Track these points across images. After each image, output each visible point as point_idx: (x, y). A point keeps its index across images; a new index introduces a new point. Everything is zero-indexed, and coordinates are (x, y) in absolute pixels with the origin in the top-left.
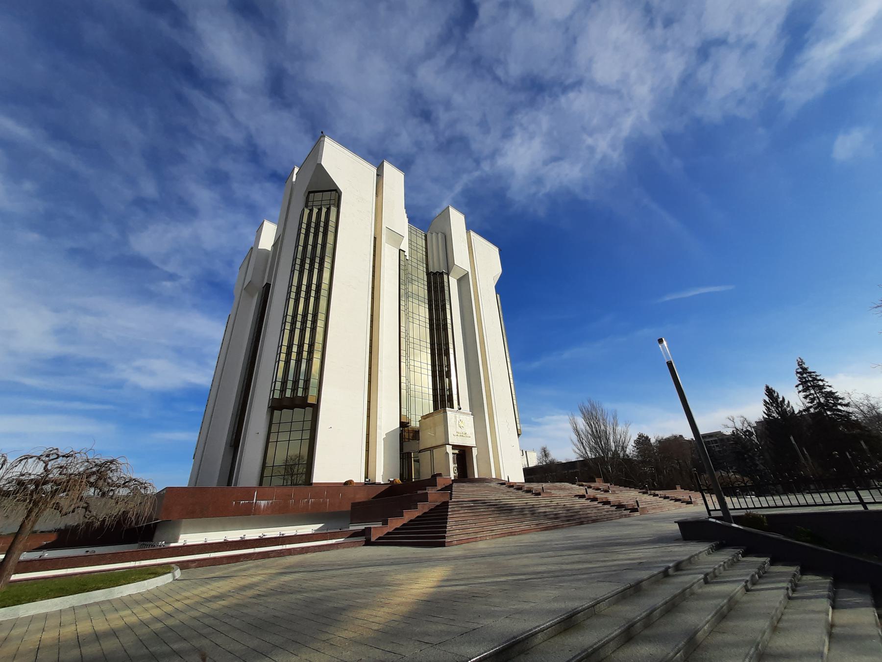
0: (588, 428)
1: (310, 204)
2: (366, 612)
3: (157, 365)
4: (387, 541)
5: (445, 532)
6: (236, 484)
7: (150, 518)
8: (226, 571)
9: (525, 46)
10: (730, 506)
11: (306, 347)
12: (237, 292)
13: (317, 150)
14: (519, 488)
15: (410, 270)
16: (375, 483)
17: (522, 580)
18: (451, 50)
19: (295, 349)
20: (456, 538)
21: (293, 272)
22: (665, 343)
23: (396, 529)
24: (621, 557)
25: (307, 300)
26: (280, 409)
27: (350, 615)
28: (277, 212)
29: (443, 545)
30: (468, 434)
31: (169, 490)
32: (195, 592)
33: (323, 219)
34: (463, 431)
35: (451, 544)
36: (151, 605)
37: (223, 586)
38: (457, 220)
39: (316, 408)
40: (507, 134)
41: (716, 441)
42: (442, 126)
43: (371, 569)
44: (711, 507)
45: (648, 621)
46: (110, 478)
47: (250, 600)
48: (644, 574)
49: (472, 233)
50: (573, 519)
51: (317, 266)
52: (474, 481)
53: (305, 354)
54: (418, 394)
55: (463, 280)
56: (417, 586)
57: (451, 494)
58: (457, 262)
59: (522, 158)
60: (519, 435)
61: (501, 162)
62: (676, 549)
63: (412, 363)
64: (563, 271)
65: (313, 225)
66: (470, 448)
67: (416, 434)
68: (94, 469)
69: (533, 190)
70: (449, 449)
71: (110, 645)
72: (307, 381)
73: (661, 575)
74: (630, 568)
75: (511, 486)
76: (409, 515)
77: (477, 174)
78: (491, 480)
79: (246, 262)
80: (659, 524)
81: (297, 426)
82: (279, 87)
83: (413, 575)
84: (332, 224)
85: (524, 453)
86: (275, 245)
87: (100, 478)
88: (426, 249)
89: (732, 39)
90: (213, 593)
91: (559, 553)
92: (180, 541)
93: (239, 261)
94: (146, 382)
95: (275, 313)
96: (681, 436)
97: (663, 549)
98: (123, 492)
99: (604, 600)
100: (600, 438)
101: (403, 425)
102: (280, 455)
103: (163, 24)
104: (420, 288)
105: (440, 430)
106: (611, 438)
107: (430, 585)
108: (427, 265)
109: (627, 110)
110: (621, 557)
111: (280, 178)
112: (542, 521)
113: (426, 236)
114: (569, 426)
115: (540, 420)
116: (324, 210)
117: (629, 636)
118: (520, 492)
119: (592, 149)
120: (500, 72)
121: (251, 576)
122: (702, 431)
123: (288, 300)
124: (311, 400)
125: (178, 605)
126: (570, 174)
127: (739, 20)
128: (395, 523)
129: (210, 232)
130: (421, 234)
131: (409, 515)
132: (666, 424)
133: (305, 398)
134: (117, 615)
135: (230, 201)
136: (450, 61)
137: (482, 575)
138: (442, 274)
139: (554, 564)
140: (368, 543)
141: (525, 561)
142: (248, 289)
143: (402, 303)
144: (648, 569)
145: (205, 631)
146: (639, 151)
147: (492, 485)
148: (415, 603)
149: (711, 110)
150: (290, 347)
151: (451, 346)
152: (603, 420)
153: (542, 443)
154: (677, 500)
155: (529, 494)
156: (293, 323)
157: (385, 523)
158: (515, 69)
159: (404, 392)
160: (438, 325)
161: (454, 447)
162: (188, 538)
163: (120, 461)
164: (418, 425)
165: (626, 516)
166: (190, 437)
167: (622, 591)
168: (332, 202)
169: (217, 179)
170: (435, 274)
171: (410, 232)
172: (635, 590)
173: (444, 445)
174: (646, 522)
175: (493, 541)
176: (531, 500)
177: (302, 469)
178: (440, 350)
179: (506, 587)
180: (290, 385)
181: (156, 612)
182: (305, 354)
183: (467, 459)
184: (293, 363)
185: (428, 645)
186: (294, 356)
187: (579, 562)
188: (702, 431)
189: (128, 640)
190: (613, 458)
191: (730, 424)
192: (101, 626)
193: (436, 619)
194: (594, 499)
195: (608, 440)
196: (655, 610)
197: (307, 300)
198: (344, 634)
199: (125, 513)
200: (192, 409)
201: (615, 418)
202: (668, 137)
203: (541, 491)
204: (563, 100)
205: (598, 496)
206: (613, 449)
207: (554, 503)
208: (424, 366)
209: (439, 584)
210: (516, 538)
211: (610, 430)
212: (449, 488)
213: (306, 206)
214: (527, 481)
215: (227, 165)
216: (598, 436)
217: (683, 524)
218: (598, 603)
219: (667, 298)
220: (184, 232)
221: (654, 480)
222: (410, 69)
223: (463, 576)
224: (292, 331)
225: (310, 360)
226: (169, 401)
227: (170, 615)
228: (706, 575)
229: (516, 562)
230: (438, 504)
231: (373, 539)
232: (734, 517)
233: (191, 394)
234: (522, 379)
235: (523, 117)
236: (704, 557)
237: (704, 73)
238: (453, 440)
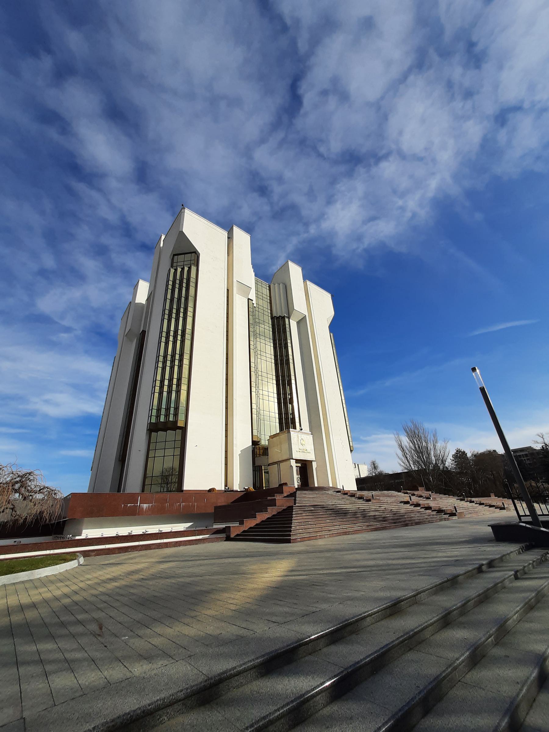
0: (411, 444)
1: (175, 264)
2: (226, 595)
3: (60, 398)
4: (243, 537)
5: (290, 531)
6: (124, 490)
7: (60, 517)
8: (117, 560)
9: (342, 126)
10: (539, 512)
11: (175, 381)
12: (120, 340)
13: (178, 219)
14: (353, 495)
15: (257, 316)
16: (233, 491)
17: (354, 572)
18: (280, 135)
19: (166, 382)
20: (299, 536)
21: (163, 320)
22: (478, 371)
23: (251, 528)
24: (440, 554)
25: (175, 343)
26: (156, 431)
27: (213, 597)
28: (148, 274)
29: (289, 541)
30: (309, 450)
31: (74, 495)
32: (95, 575)
33: (185, 276)
34: (304, 447)
35: (295, 541)
36: (62, 584)
37: (116, 571)
38: (295, 272)
39: (184, 430)
40: (330, 201)
41: (526, 455)
42: (275, 198)
43: (230, 560)
44: (522, 513)
45: (464, 609)
46: (29, 486)
47: (136, 583)
48: (460, 570)
49: (308, 283)
50: (400, 521)
51: (181, 315)
52: (314, 489)
53: (174, 387)
54: (267, 418)
55: (302, 322)
56: (267, 575)
57: (295, 500)
59: (344, 219)
60: (351, 451)
61: (325, 225)
62: (489, 549)
63: (261, 392)
64: (389, 311)
66: (311, 462)
68: (18, 479)
69: (354, 246)
70: (293, 463)
71: (31, 615)
72: (177, 409)
73: (475, 571)
74: (448, 564)
75: (345, 493)
76: (261, 517)
77: (305, 235)
78: (328, 489)
79: (127, 311)
80: (475, 527)
81: (170, 445)
82: (143, 175)
83: (263, 566)
84: (193, 280)
85: (356, 466)
86: (148, 300)
87: (22, 486)
88: (270, 297)
89: (526, 105)
90: (109, 576)
91: (386, 550)
92: (83, 535)
93: (119, 315)
94: (53, 411)
95: (150, 353)
96: (495, 451)
97: (477, 549)
98: (39, 496)
99: (424, 591)
100: (422, 453)
101: (255, 443)
103: (53, 133)
104: (267, 328)
105: (285, 446)
106: (432, 453)
107: (278, 574)
108: (271, 310)
109: (433, 174)
110: (440, 554)
111: (148, 247)
112: (371, 523)
113: (269, 287)
114: (395, 444)
115: (368, 438)
116: (186, 269)
117: (447, 621)
118: (353, 498)
119: (403, 209)
120: (322, 149)
121: (136, 563)
122: (512, 447)
124: (181, 424)
125: (82, 585)
126: (385, 230)
127: (532, 88)
128: (250, 523)
129: (96, 292)
130: (265, 285)
131: (261, 517)
132: (481, 441)
133: (176, 422)
134: (36, 592)
135: (110, 268)
136: (282, 143)
137: (320, 567)
138: (283, 318)
139: (382, 559)
140: (228, 539)
141: (358, 557)
142: (128, 335)
143: (252, 343)
144: (464, 565)
145: (102, 606)
146: (443, 206)
147: (330, 492)
148: (264, 589)
149: (509, 166)
150: (162, 381)
152: (425, 437)
153: (370, 458)
154: (491, 506)
155: (361, 500)
156: (164, 362)
157: (242, 523)
158: (335, 146)
159: (254, 416)
160: (282, 360)
161: (297, 461)
162: (89, 532)
163: (36, 472)
164: (267, 444)
165: (445, 519)
166: (88, 454)
167: (440, 584)
169: (100, 251)
170: (278, 318)
171: (256, 284)
172: (452, 583)
173: (289, 459)
174: (462, 525)
175: (331, 539)
176: (361, 505)
177: (175, 479)
178: (283, 381)
179: (339, 578)
180: (163, 412)
181: (66, 590)
182: (174, 387)
184: (165, 394)
185: (275, 624)
186: (166, 389)
187: (403, 558)
188: (512, 447)
189: (44, 611)
190: (434, 470)
191: (540, 440)
192: (25, 599)
193: (282, 603)
194: (417, 505)
195: (429, 454)
196: (469, 601)
197: (175, 343)
198: (209, 612)
199: (41, 513)
200: (88, 432)
201: (435, 435)
202: (470, 194)
203: (371, 498)
204: (374, 170)
205: (421, 502)
206: (434, 462)
209: (285, 574)
210: (349, 537)
211: (430, 446)
212: (293, 495)
213: (172, 266)
214: (359, 489)
215: (106, 240)
216: (421, 452)
217: (495, 527)
218: (417, 594)
219: (477, 333)
220: (76, 294)
221: (470, 489)
222: (248, 152)
223: (304, 568)
224: (164, 369)
225: (178, 392)
226: (71, 425)
227: (76, 593)
228: (516, 572)
229: (349, 556)
230: (285, 508)
231: (232, 536)
232: (542, 522)
233: (87, 420)
234: (352, 404)
235: (341, 186)
236: (513, 556)
237: (502, 136)
238: (297, 455)
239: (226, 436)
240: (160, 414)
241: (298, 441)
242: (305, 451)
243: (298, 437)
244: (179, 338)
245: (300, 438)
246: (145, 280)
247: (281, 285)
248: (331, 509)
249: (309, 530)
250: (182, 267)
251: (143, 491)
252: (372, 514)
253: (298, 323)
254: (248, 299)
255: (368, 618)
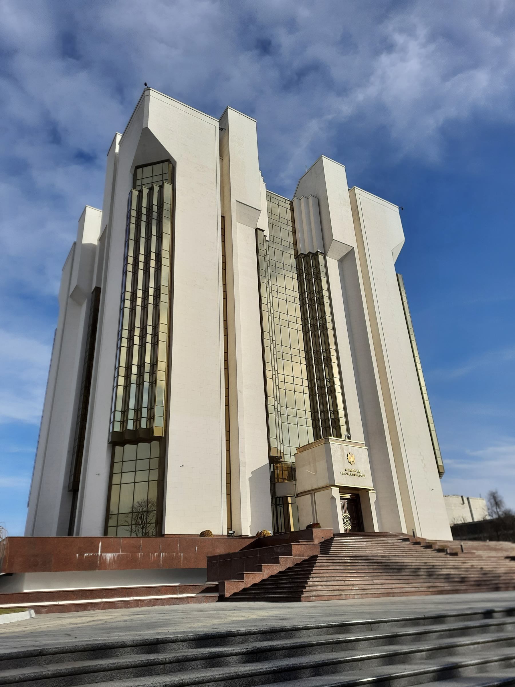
1: (139, 183)
6: (78, 533)
13: (140, 109)
16: (241, 536)
19: (140, 294)
30: (362, 472)
38: (334, 174)
39: (163, 441)
49: (358, 191)
55: (347, 260)
58: (337, 235)
60: (440, 474)
63: (281, 377)
65: (144, 211)
67: (291, 473)
70: (335, 492)
76: (269, 571)
79: (70, 260)
88: (293, 222)
95: (109, 319)
101: (274, 460)
102: (127, 499)
113: (292, 204)
116: (156, 189)
123: (125, 272)
124: (158, 432)
131: (269, 571)
133: (150, 430)
140: (222, 599)
142: (74, 296)
150: (128, 368)
151: (333, 353)
161: (343, 489)
164: (293, 461)
168: (165, 177)
173: (328, 487)
180: (131, 414)
183: (363, 507)
207: (468, 565)
208: (298, 381)
213: (134, 186)
224: (130, 348)
230: (306, 558)
231: (228, 595)
234: (442, 393)
238: (341, 480)
239: (228, 450)
240: (127, 419)
241: (343, 456)
242: (356, 473)
243: (342, 449)
244: (151, 305)
245: (346, 452)
246: (95, 206)
247: (310, 199)
248: (378, 563)
249: (332, 588)
250: (150, 186)
251: (106, 533)
252: (445, 572)
253: (341, 262)
254: (257, 229)
255: (304, 631)
